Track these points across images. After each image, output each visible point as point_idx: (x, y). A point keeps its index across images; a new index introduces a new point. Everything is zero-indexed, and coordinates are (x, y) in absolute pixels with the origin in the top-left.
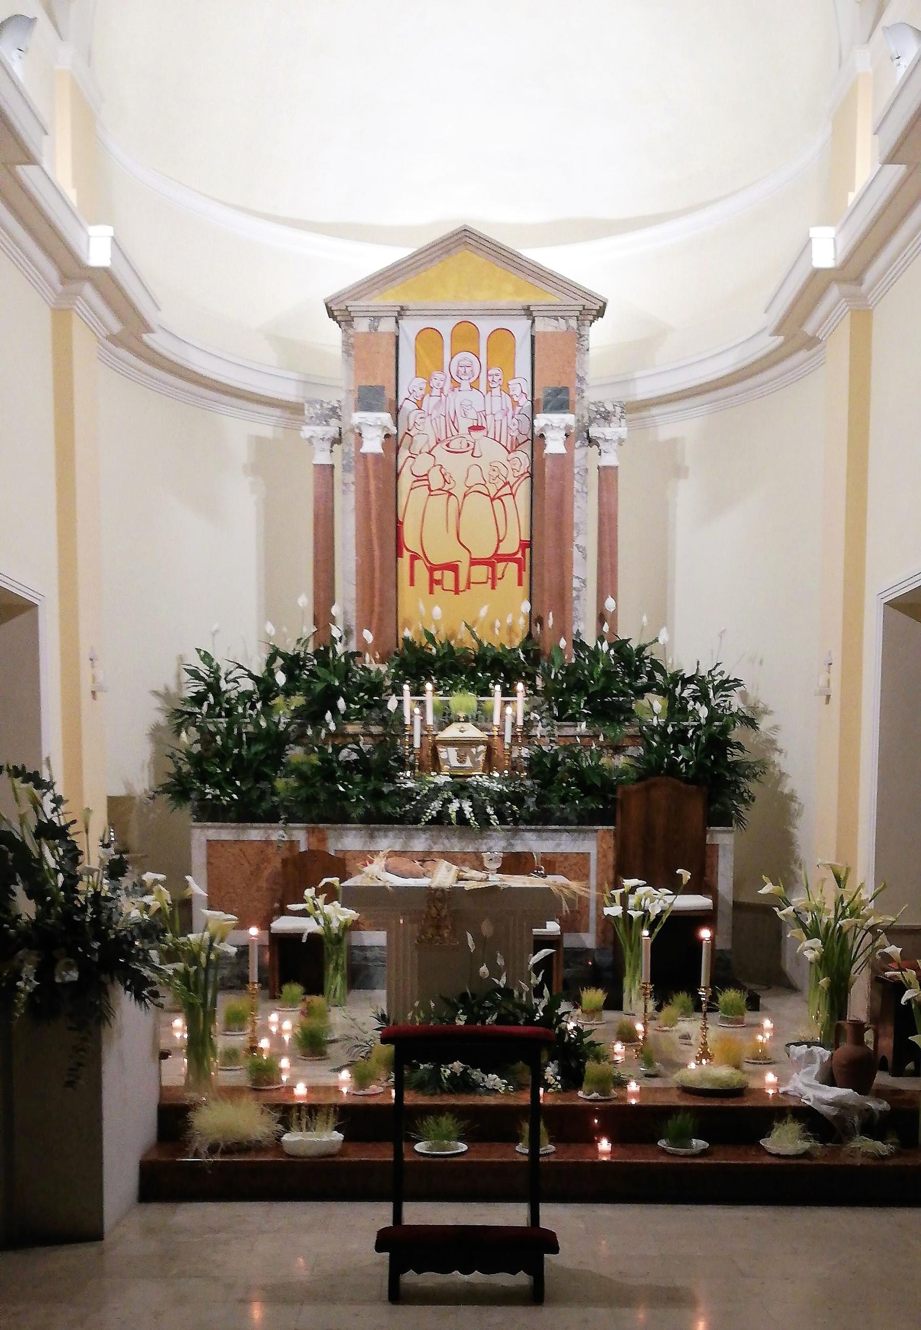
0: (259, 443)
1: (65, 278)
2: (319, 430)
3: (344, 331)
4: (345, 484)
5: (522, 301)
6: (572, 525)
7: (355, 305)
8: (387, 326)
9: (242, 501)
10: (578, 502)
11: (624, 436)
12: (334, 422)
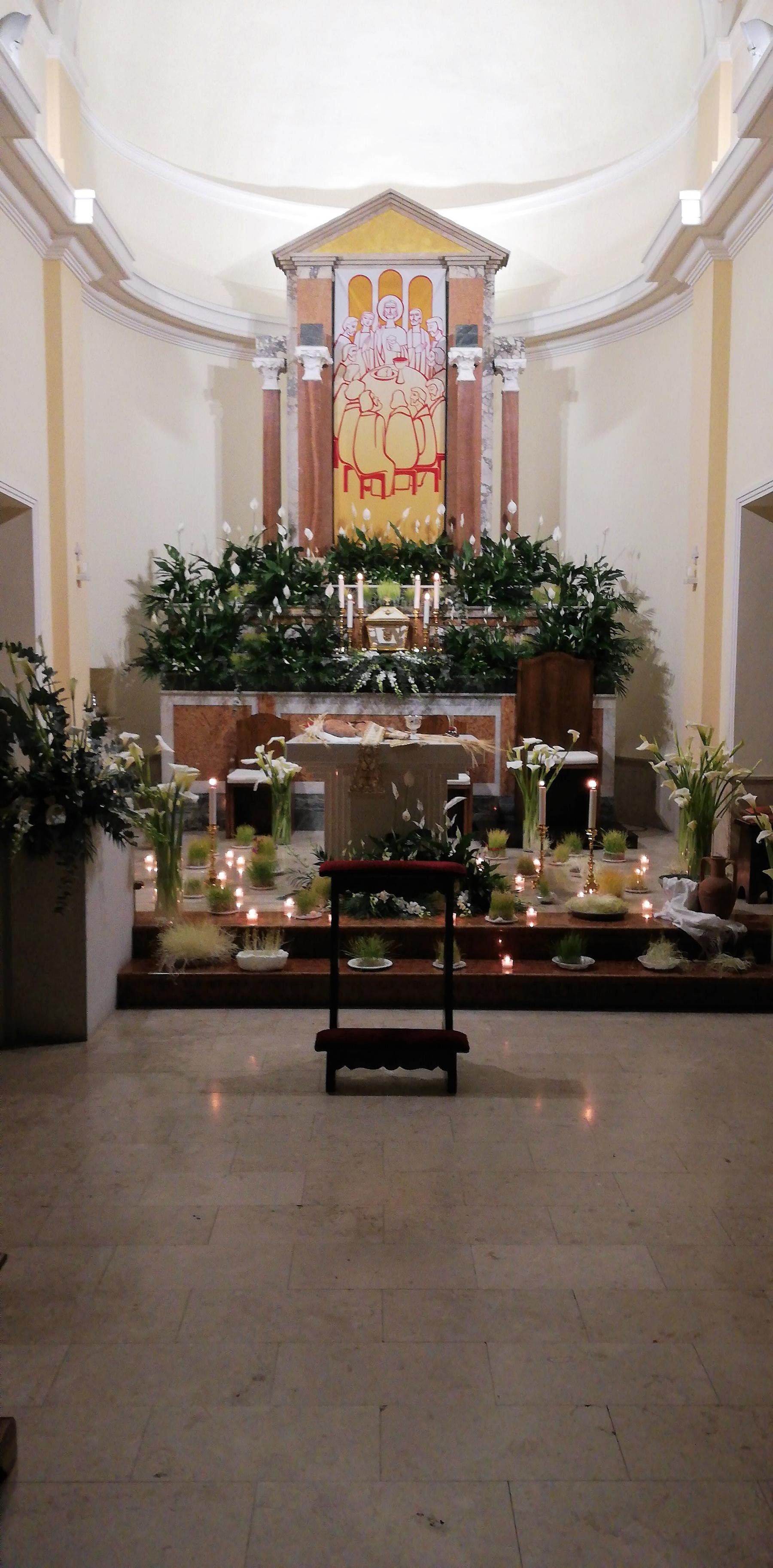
0: (218, 371)
1: (55, 233)
2: (268, 361)
3: (289, 278)
4: (289, 406)
5: (438, 252)
6: (480, 441)
7: (297, 256)
8: (325, 273)
9: (204, 421)
10: (485, 421)
11: (524, 366)
12: (280, 354)
